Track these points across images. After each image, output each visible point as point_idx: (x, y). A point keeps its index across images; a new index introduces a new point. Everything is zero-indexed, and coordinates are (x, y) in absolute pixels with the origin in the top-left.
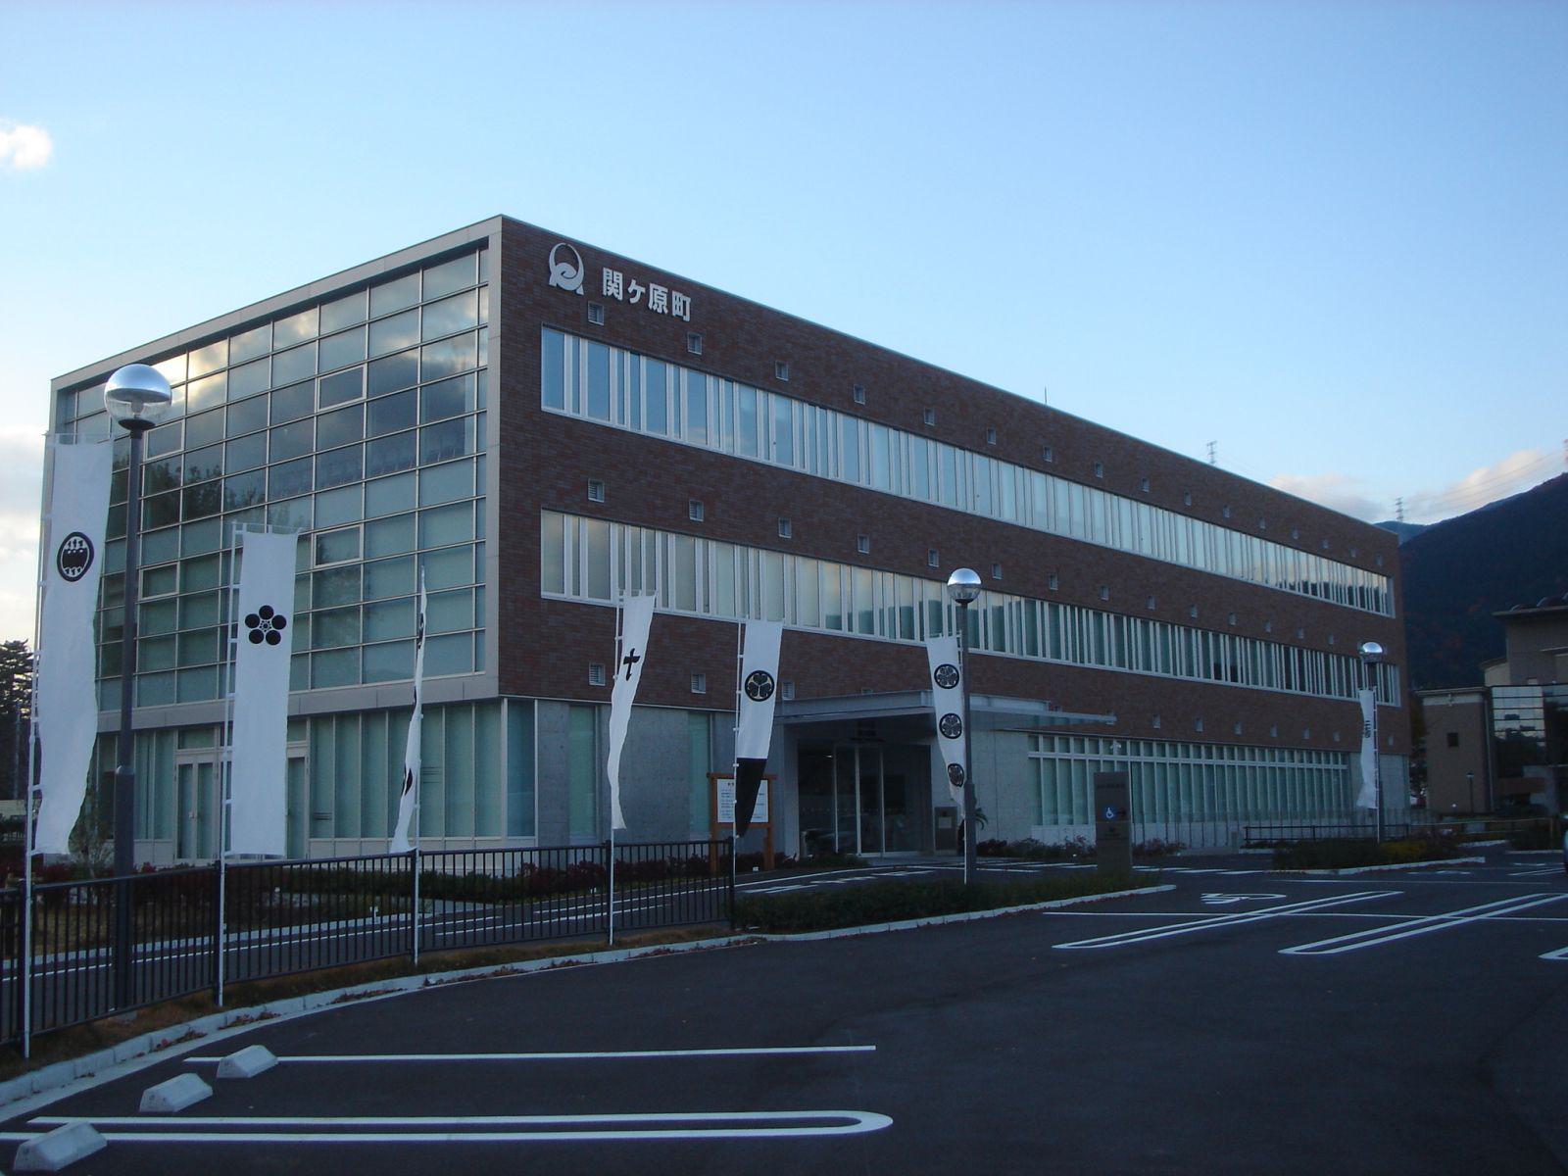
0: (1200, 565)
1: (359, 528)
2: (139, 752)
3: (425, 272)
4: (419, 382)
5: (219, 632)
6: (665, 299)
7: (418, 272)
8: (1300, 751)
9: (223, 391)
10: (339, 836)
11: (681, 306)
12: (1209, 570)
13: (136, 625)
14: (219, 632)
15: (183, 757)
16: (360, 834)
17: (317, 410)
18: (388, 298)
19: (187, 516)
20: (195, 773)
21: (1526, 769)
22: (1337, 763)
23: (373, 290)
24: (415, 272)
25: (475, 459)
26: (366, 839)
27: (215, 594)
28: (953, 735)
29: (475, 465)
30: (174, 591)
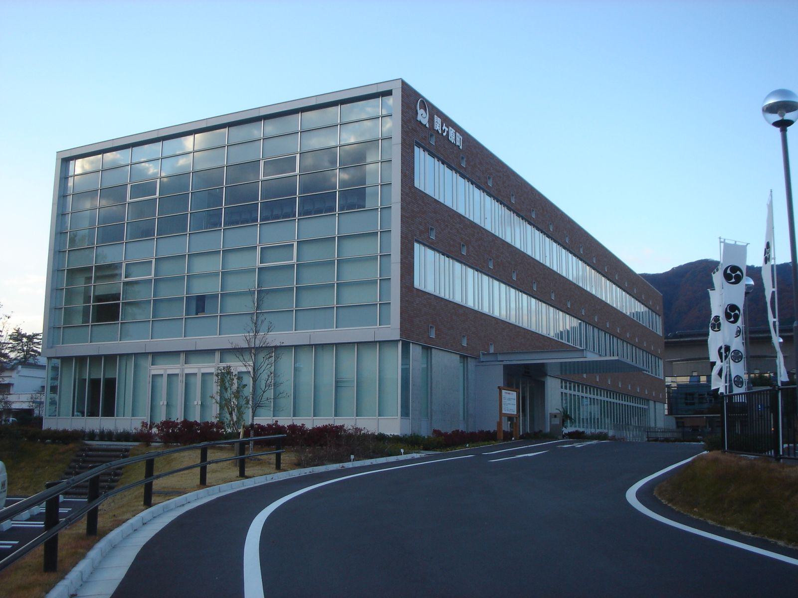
0: (470, 304)
1: (152, 261)
2: (120, 369)
3: (229, 128)
4: (224, 184)
5: (152, 302)
6: (454, 135)
7: (226, 128)
8: (570, 382)
9: (191, 163)
10: (133, 416)
11: (458, 140)
12: (476, 308)
13: (91, 297)
14: (152, 302)
15: (156, 370)
16: (131, 415)
17: (128, 200)
18: (258, 131)
19: (341, 209)
20: (164, 381)
21: (514, 395)
22: (575, 391)
23: (230, 128)
24: (297, 113)
25: (155, 239)
26: (134, 418)
27: (333, 262)
28: (737, 361)
29: (155, 242)
30: (151, 275)
